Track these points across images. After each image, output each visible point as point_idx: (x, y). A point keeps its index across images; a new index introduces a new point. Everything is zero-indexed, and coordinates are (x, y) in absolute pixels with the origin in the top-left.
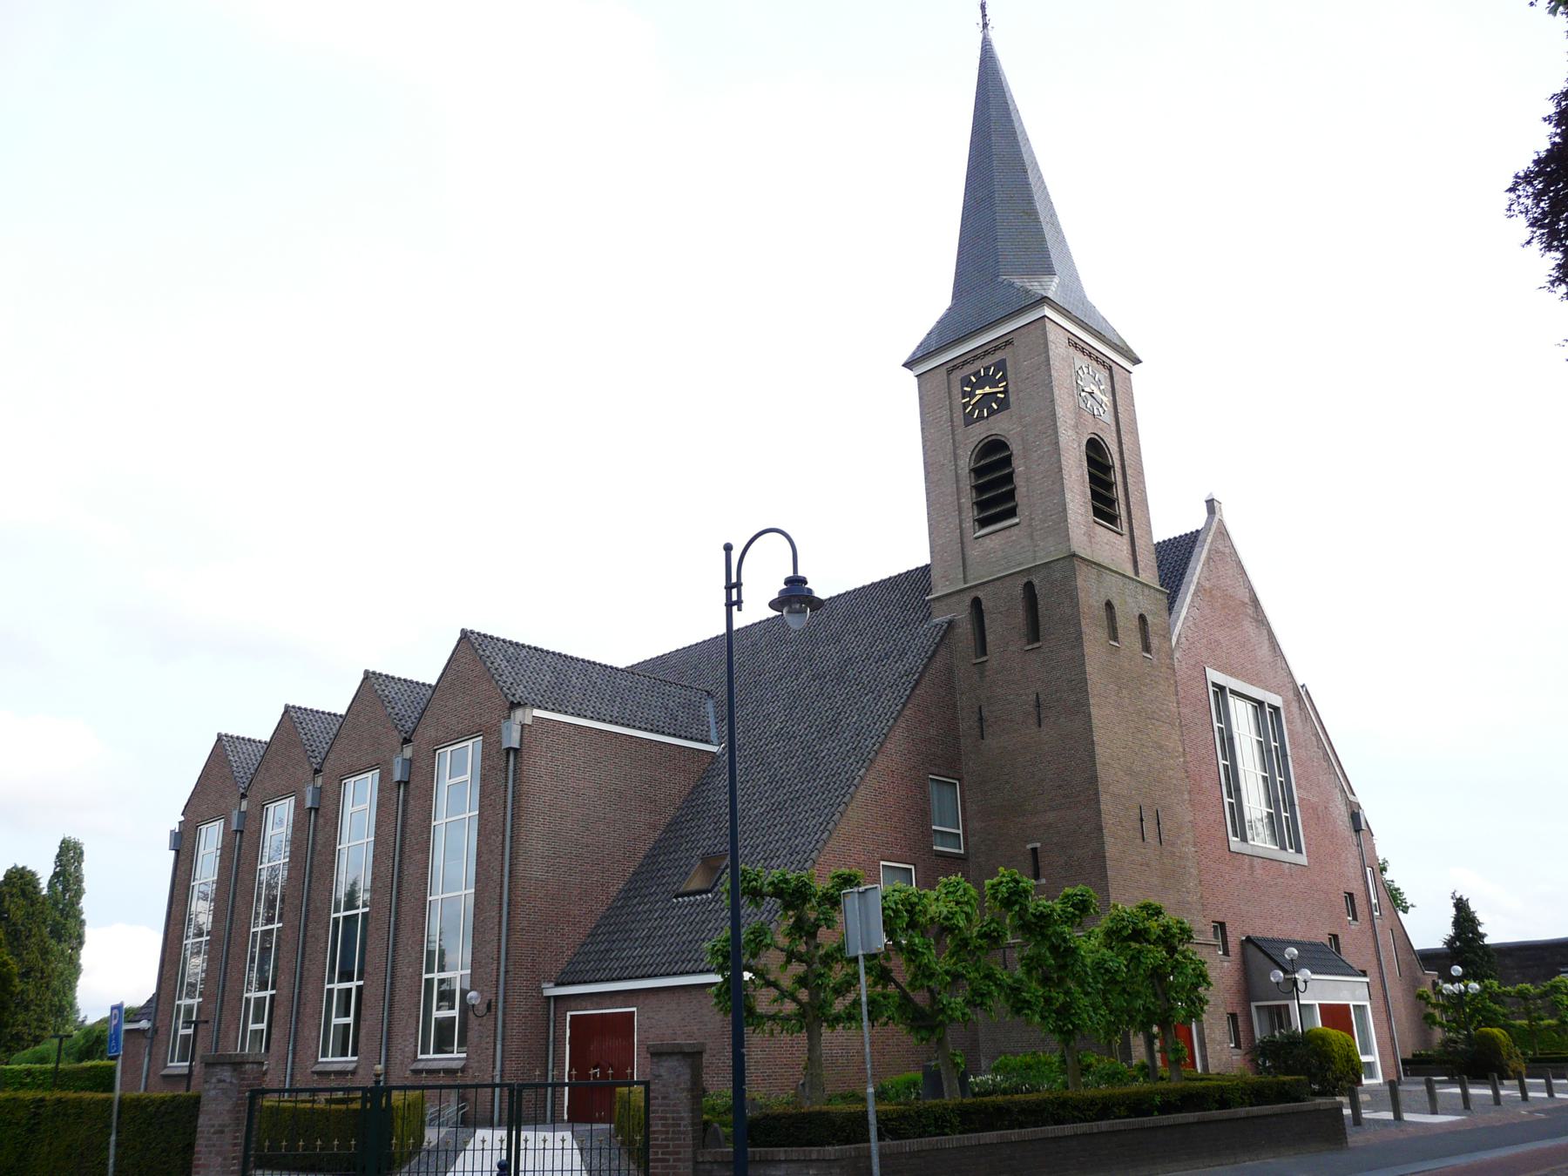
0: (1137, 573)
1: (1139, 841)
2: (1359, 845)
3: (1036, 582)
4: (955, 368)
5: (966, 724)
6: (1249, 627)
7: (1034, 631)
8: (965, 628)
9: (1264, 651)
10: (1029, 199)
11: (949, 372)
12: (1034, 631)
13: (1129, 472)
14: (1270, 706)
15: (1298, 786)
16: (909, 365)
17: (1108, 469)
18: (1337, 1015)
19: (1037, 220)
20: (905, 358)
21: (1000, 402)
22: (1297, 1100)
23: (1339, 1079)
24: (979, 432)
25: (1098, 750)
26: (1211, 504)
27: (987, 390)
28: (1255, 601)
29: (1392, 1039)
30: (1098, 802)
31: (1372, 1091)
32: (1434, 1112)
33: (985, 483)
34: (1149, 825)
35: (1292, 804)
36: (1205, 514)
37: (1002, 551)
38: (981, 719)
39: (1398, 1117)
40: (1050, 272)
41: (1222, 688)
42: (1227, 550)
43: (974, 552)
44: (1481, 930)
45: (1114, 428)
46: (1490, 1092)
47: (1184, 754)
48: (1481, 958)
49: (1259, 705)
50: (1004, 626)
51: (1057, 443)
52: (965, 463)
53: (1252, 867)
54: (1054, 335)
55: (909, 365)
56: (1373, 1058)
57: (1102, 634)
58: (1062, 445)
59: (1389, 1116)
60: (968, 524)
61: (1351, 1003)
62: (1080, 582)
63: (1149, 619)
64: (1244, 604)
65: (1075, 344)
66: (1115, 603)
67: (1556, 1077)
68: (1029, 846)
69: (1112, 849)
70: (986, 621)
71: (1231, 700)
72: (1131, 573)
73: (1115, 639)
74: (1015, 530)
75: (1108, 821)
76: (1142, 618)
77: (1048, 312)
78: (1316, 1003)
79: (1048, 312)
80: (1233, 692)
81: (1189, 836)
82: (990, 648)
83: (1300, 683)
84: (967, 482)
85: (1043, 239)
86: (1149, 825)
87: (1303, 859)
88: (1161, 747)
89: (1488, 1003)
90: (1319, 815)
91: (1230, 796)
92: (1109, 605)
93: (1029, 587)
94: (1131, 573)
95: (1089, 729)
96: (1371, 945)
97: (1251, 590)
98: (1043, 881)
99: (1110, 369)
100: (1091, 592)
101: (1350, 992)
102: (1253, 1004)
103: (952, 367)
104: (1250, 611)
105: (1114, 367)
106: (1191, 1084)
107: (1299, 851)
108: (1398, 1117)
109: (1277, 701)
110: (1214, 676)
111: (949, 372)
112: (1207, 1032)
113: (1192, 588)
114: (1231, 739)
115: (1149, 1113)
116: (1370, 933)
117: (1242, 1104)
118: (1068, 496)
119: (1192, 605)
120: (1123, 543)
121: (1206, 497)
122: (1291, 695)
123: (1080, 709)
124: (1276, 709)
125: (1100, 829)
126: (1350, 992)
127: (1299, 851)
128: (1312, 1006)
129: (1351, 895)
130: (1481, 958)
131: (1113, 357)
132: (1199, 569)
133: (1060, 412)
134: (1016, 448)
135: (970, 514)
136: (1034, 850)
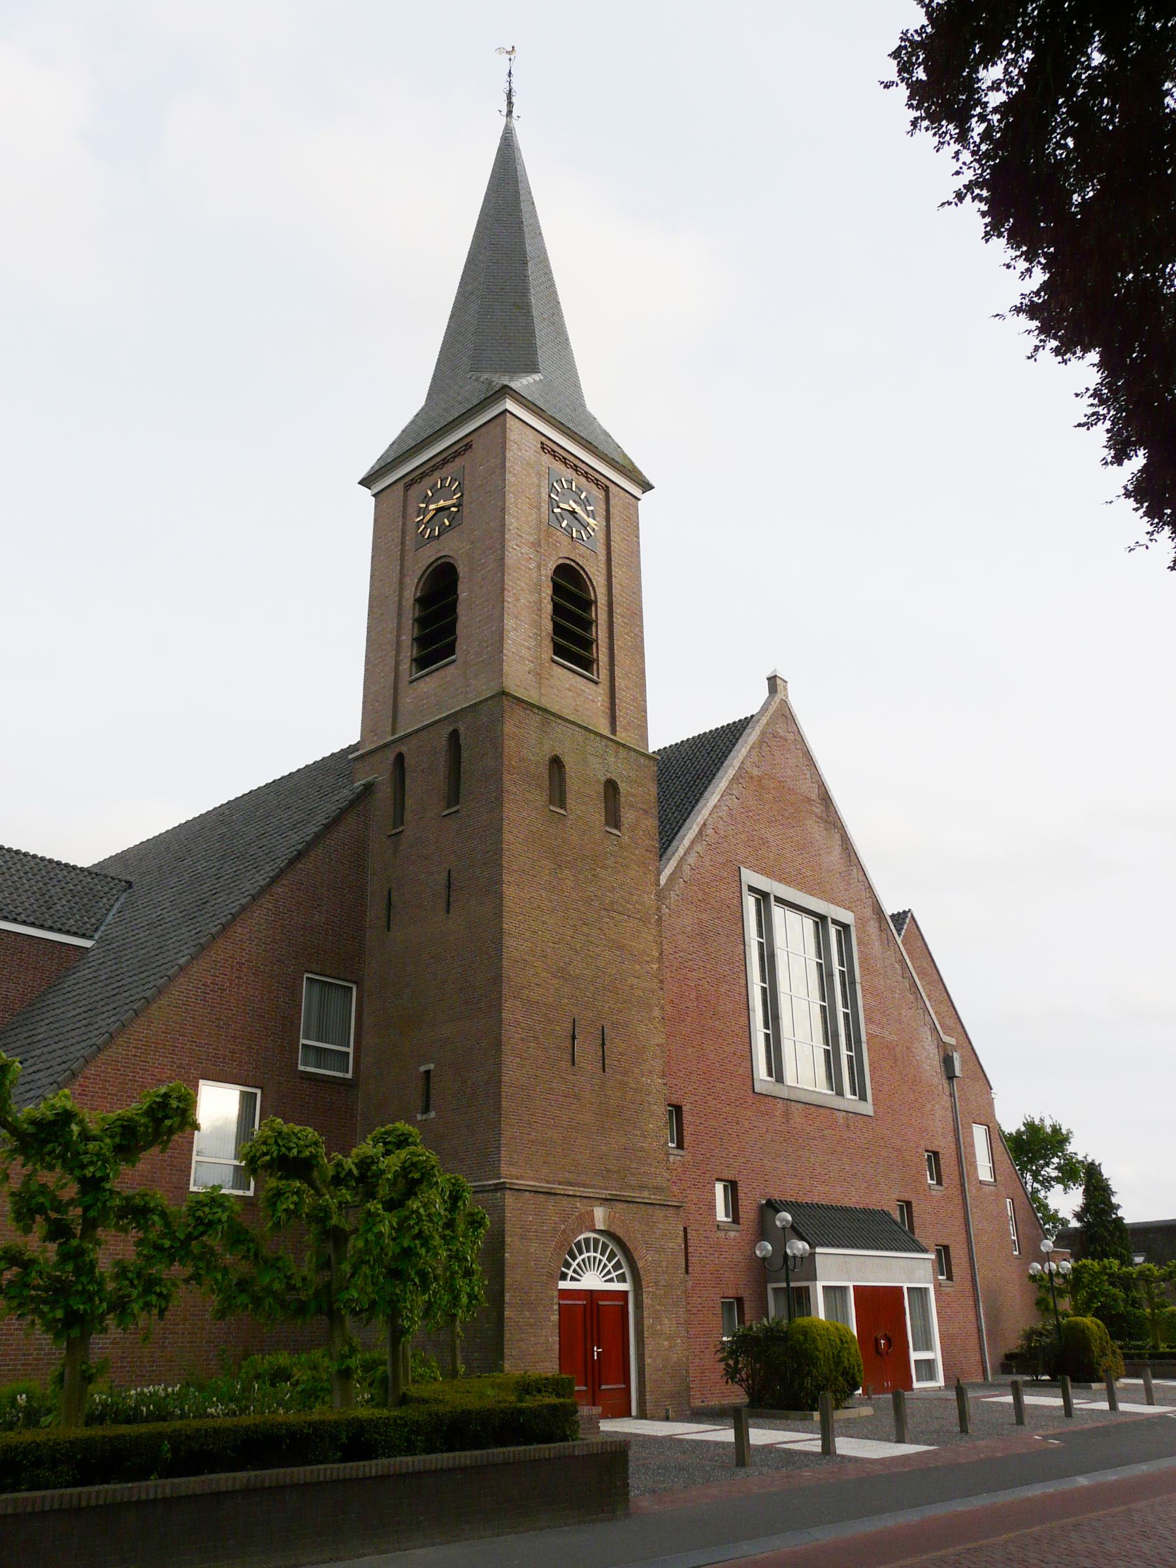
0: (614, 732)
1: (565, 1065)
2: (952, 1095)
3: (462, 730)
4: (413, 482)
5: (374, 912)
6: (815, 829)
7: (454, 796)
8: (385, 792)
9: (835, 857)
10: (523, 292)
11: (408, 487)
12: (454, 796)
13: (617, 610)
14: (835, 922)
15: (869, 1021)
16: (366, 482)
17: (587, 604)
18: (881, 1306)
19: (528, 314)
20: (362, 473)
21: (452, 518)
22: (548, 1439)
23: (820, 1388)
24: (429, 555)
25: (508, 941)
26: (773, 682)
27: (442, 503)
28: (826, 799)
29: (979, 1330)
30: (499, 1010)
31: (928, 1398)
32: (1150, 1402)
33: (427, 614)
34: (586, 1050)
35: (859, 1041)
36: (765, 693)
37: (439, 694)
38: (390, 904)
39: (1113, 1407)
40: (533, 368)
41: (763, 897)
42: (791, 737)
43: (407, 700)
44: (1114, 1200)
45: (602, 557)
46: (1059, 1402)
47: (660, 959)
48: (1112, 1235)
49: (821, 920)
50: (424, 787)
51: (502, 559)
52: (411, 593)
53: (787, 1114)
54: (514, 431)
55: (366, 482)
56: (935, 1354)
57: (539, 797)
58: (509, 561)
59: (1105, 1406)
60: (405, 665)
61: (905, 1286)
62: (509, 727)
63: (623, 787)
64: (809, 800)
65: (549, 448)
66: (568, 761)
67: (1155, 1377)
68: (422, 1069)
69: (513, 1071)
70: (407, 782)
71: (778, 912)
72: (606, 732)
73: (563, 805)
74: (451, 669)
75: (512, 1035)
76: (611, 787)
77: (510, 405)
78: (851, 1284)
79: (510, 405)
80: (778, 900)
81: (658, 1065)
82: (408, 816)
83: (891, 907)
84: (410, 612)
85: (533, 334)
86: (586, 1050)
87: (867, 1108)
88: (621, 947)
89: (1106, 1286)
90: (894, 1056)
91: (849, 1049)
92: (556, 763)
93: (454, 735)
94: (606, 732)
95: (499, 915)
96: (959, 1214)
97: (822, 786)
98: (433, 1114)
99: (606, 489)
100: (525, 745)
101: (906, 1271)
102: (770, 1286)
103: (410, 481)
104: (818, 809)
105: (612, 487)
106: (124, 1429)
107: (863, 1098)
108: (1113, 1407)
109: (847, 917)
110: (751, 877)
111: (408, 487)
112: (647, 1322)
113: (731, 773)
114: (772, 956)
115: (142, 1474)
116: (958, 1201)
117: (410, 1450)
118: (509, 623)
119: (728, 791)
120: (597, 696)
121: (769, 674)
122: (868, 912)
123: (493, 889)
124: (846, 927)
125: (499, 1044)
126: (906, 1271)
127: (863, 1098)
128: (844, 1289)
129: (936, 1154)
130: (1112, 1235)
131: (613, 480)
132: (744, 751)
133: (511, 522)
134: (462, 570)
135: (409, 651)
136: (428, 1072)
